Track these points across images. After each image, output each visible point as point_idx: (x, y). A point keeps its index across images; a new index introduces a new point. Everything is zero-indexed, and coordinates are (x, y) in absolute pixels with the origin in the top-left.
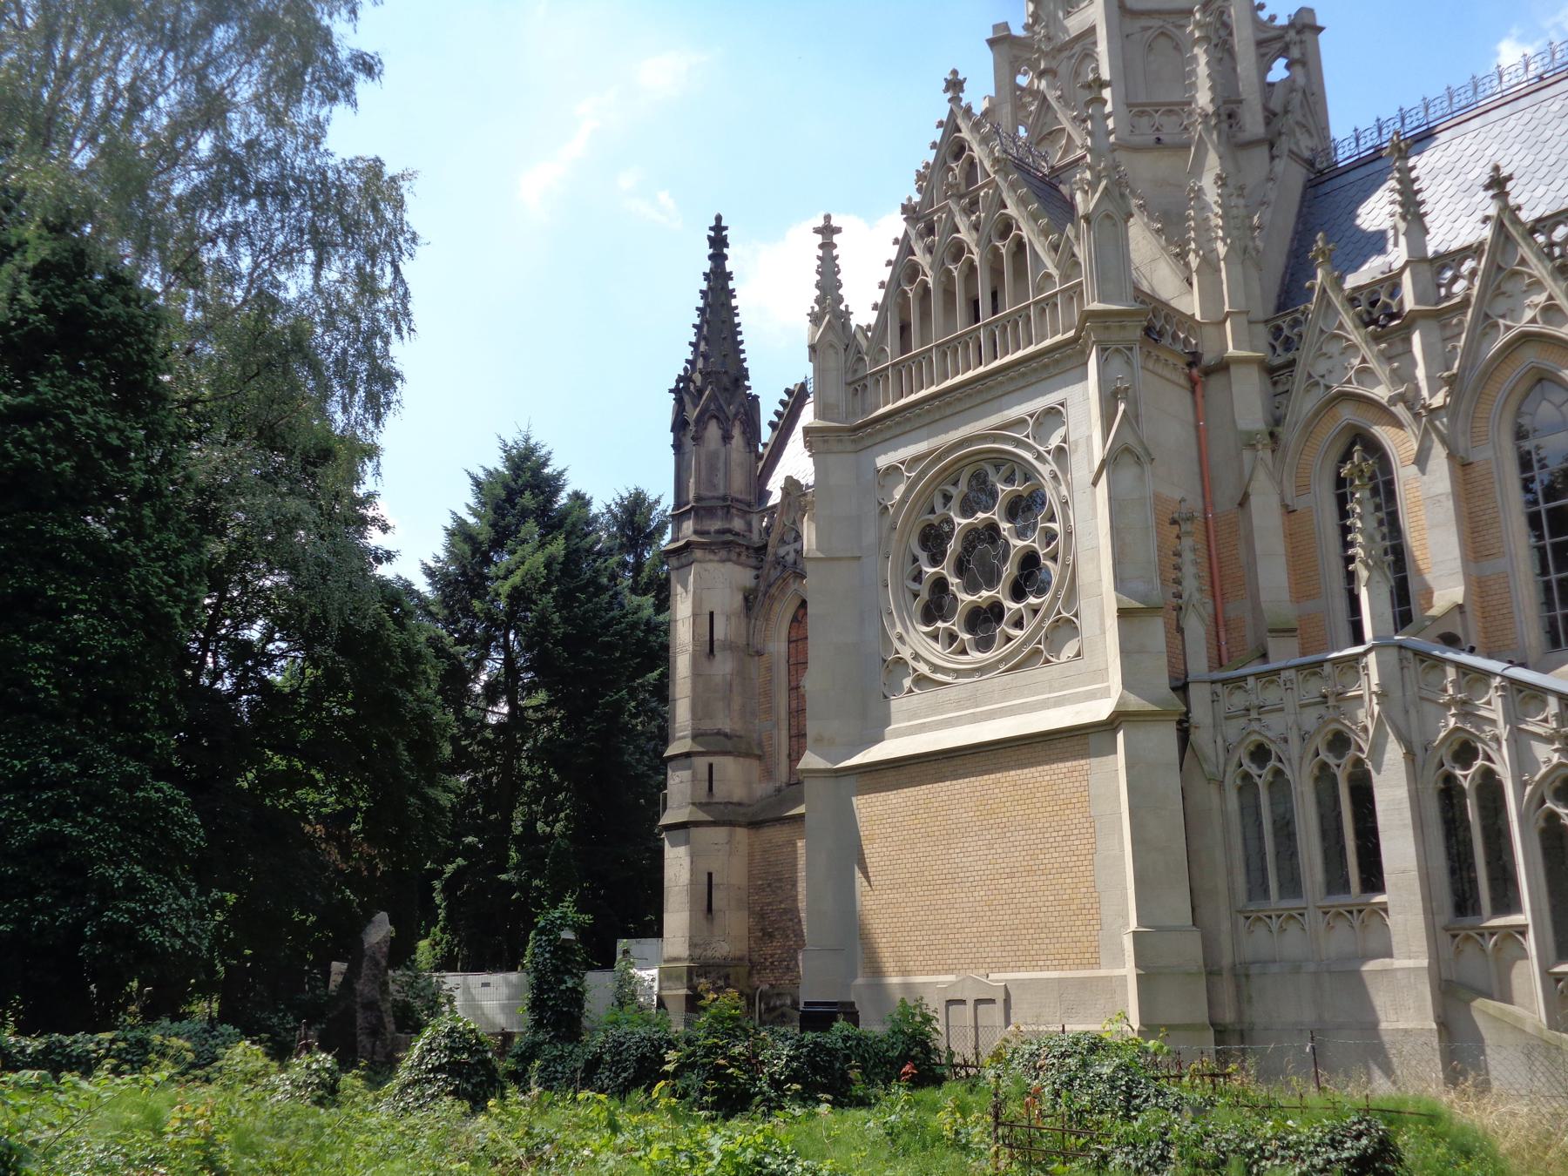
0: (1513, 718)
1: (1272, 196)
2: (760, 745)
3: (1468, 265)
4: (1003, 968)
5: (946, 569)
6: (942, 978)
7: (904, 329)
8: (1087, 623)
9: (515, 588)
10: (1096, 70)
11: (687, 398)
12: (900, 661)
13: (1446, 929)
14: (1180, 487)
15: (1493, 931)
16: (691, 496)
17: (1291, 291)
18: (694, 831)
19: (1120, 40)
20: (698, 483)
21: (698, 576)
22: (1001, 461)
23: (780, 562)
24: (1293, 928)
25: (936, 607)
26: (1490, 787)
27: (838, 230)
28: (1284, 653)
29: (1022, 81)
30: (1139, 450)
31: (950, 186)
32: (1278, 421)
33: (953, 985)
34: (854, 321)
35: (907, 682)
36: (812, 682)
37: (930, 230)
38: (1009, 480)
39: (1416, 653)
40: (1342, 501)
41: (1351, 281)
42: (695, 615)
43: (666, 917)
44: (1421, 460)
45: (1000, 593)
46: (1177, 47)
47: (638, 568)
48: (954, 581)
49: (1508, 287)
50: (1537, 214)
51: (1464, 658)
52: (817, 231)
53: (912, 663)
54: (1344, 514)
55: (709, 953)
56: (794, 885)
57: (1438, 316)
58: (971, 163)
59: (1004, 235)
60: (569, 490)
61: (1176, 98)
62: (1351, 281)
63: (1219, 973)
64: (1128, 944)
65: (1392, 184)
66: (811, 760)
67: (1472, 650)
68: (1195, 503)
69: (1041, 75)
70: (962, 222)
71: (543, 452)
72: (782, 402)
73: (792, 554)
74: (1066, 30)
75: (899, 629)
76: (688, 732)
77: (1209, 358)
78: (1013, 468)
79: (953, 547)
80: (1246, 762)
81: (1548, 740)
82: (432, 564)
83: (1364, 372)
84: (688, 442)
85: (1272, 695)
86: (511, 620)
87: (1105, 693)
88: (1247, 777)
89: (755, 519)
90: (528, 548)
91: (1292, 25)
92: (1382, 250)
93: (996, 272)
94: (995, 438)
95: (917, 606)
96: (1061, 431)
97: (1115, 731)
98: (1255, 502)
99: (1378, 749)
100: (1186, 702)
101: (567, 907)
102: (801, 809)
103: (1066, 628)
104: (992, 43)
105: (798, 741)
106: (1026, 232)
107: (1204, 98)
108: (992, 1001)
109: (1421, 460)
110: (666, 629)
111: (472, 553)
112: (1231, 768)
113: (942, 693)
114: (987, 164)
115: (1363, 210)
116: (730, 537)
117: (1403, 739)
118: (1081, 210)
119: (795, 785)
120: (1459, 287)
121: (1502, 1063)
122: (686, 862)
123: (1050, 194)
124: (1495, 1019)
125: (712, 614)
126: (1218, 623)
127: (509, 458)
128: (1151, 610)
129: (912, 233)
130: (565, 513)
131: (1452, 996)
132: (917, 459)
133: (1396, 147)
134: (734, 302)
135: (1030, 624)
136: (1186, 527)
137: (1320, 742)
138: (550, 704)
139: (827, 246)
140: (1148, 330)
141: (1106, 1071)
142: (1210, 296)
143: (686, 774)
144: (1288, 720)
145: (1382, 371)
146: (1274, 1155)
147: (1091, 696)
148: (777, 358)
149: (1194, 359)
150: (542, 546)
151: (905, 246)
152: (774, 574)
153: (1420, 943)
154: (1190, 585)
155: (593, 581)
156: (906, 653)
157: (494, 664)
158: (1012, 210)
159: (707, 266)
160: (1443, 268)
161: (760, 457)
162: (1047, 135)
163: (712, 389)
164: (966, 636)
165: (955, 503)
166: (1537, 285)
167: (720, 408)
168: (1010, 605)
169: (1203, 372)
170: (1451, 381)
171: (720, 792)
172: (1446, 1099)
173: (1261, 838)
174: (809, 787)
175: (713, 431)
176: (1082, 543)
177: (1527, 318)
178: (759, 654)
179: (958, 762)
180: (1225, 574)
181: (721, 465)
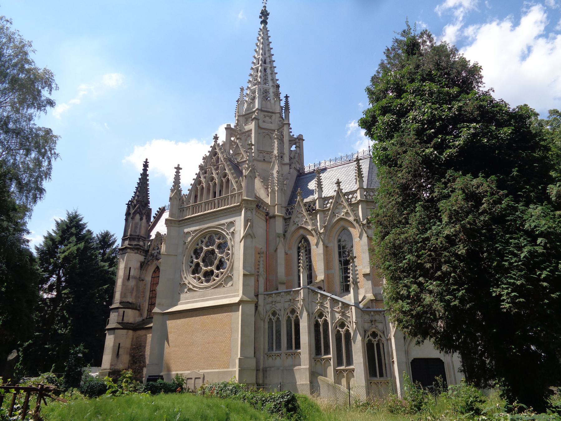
0: (332, 307)
1: (289, 177)
2: (140, 307)
3: (331, 201)
4: (203, 369)
5: (200, 260)
6: (186, 372)
7: (196, 197)
8: (235, 277)
9: (65, 256)
10: (251, 141)
11: (131, 207)
12: (185, 284)
13: (313, 358)
14: (260, 244)
15: (324, 359)
16: (129, 234)
17: (291, 201)
18: (116, 331)
19: (257, 134)
20: (131, 231)
21: (128, 257)
22: (217, 233)
23: (152, 255)
24: (278, 358)
25: (196, 270)
26: (326, 323)
27: (181, 169)
28: (282, 289)
29: (232, 139)
30: (252, 235)
31: (212, 163)
32: (286, 232)
33: (189, 374)
34: (183, 193)
35: (186, 290)
36: (159, 288)
37: (206, 173)
38: (219, 239)
39: (312, 290)
40: (299, 252)
41: (306, 200)
42: (125, 268)
43: (104, 356)
44: (317, 245)
45: (213, 268)
46: (271, 138)
47: (104, 254)
48: (201, 264)
49: (339, 207)
50: (346, 191)
51: (322, 292)
52: (175, 168)
53: (188, 285)
54: (299, 256)
55: (116, 367)
56: (145, 347)
57: (323, 211)
58: (218, 157)
59: (224, 177)
60: (87, 229)
61: (269, 150)
62: (306, 200)
63: (259, 370)
64: (237, 361)
65: (316, 179)
66: (156, 310)
67: (324, 291)
68: (264, 249)
69: (237, 139)
70: (214, 172)
71: (81, 217)
72: (157, 211)
73: (156, 253)
74: (244, 129)
75: (185, 275)
76: (119, 301)
77: (271, 214)
78: (220, 236)
79: (202, 255)
80: (271, 315)
81: (339, 313)
82: (38, 246)
83: (306, 222)
84: (130, 219)
85: (278, 299)
86: (62, 266)
87: (238, 296)
88: (270, 319)
89: (146, 242)
90: (72, 245)
91: (297, 138)
92: (313, 194)
93: (221, 186)
94: (217, 228)
95: (191, 270)
96: (234, 228)
97: (239, 305)
98: (278, 251)
99: (301, 313)
100: (258, 299)
101: (81, 347)
102: (151, 325)
103: (229, 278)
104: (226, 128)
105: (152, 305)
106: (230, 177)
107: (276, 152)
108: (200, 378)
109: (317, 245)
110: (114, 274)
111: (52, 245)
112: (267, 317)
113: (195, 293)
114: (222, 159)
115: (309, 184)
116: (138, 247)
117: (307, 311)
118: (244, 174)
119: (150, 319)
120: (328, 205)
121: (323, 390)
122: (113, 340)
123: (237, 168)
124: (323, 381)
125: (130, 268)
126: (267, 280)
127: (69, 217)
128: (251, 275)
129: (201, 173)
130: (85, 236)
131: (314, 375)
132: (195, 231)
133: (317, 171)
134: (148, 183)
135: (220, 277)
136: (262, 255)
137: (288, 311)
138: (70, 293)
139: (178, 172)
140: (257, 206)
141: (231, 388)
142: (273, 199)
143: (116, 314)
144: (282, 305)
145: (310, 222)
146: (269, 401)
147: (234, 296)
148: (159, 198)
149: (267, 214)
150: (76, 245)
151: (198, 175)
152: (150, 258)
153: (307, 362)
154: (261, 270)
155: (90, 257)
156: (186, 282)
157: (54, 279)
158: (227, 171)
159: (142, 172)
160: (326, 200)
161: (150, 225)
162: (237, 153)
163: (139, 207)
164: (203, 279)
165: (204, 243)
166: (345, 207)
167: (140, 211)
168: (216, 271)
169: (269, 217)
170: (325, 227)
171: (126, 320)
172: (310, 397)
173: (272, 335)
174: (155, 317)
175: (138, 217)
176: (236, 257)
177: (342, 215)
178: (143, 280)
179: (197, 312)
180: (270, 268)
181: (139, 226)
